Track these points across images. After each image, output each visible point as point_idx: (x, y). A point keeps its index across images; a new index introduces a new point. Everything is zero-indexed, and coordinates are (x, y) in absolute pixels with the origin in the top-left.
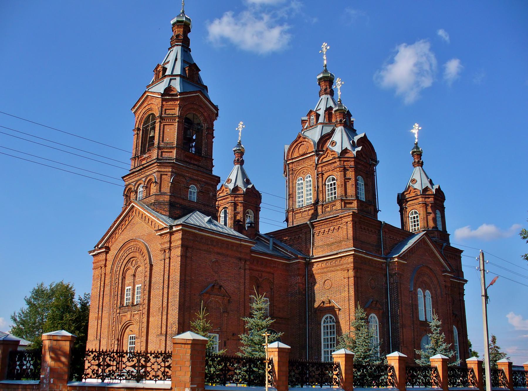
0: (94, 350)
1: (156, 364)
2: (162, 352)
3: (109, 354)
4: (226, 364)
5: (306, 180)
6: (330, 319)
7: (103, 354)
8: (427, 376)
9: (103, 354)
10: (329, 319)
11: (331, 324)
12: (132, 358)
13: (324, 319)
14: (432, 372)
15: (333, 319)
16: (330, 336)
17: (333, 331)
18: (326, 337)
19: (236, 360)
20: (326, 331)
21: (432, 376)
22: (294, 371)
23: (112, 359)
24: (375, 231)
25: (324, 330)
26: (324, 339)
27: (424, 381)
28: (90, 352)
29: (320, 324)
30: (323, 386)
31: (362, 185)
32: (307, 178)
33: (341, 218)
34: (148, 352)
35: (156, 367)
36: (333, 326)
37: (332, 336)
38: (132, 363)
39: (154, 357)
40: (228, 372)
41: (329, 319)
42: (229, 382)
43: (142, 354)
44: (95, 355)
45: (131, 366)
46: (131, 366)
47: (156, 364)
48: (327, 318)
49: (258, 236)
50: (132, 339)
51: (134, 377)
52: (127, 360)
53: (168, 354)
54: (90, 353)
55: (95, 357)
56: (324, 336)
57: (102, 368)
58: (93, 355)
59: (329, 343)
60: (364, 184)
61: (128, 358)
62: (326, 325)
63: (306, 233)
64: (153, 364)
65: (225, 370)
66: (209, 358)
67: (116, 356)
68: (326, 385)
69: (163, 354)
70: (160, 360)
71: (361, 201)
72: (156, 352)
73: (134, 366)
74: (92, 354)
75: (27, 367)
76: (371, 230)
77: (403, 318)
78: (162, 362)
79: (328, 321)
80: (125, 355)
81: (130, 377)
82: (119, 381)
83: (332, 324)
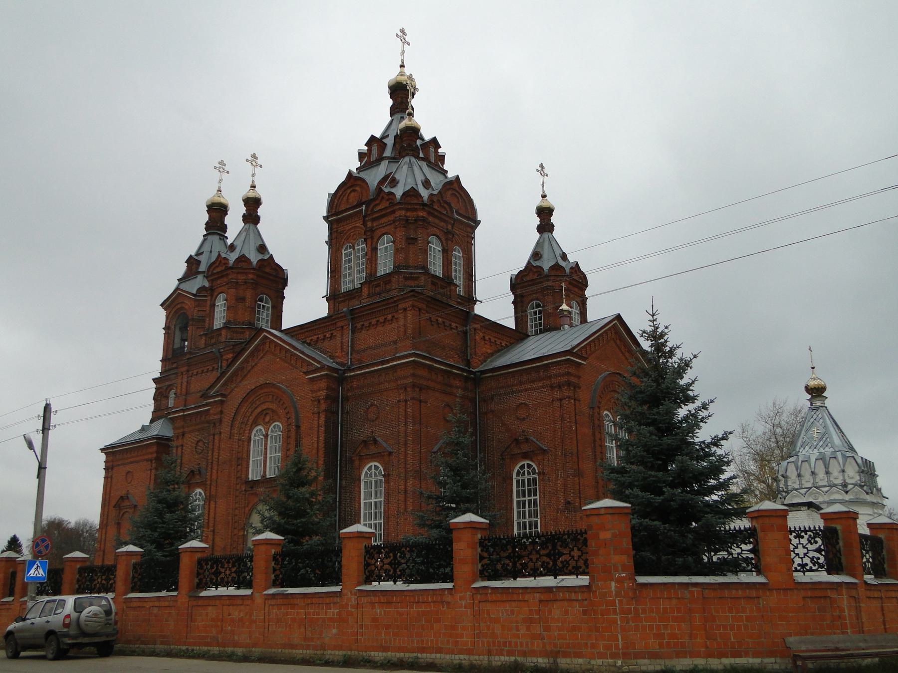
0: (807, 529)
1: (800, 546)
4: (395, 556)
5: (356, 248)
6: (527, 467)
8: (213, 574)
10: (526, 469)
11: (529, 477)
12: (814, 538)
13: (517, 468)
14: (209, 567)
15: (534, 468)
16: (529, 496)
18: (521, 499)
19: (408, 549)
20: (521, 488)
25: (518, 486)
26: (518, 502)
29: (511, 479)
30: (219, 589)
31: (439, 251)
32: (359, 245)
33: (395, 302)
36: (535, 479)
37: (532, 498)
38: (815, 546)
41: (526, 469)
47: (800, 546)
48: (522, 467)
49: (265, 333)
50: (376, 518)
54: (579, 537)
56: (518, 496)
59: (527, 509)
60: (440, 250)
62: (521, 478)
63: (342, 327)
64: (797, 548)
66: (406, 549)
70: (804, 541)
71: (434, 276)
74: (806, 534)
75: (101, 578)
78: (807, 544)
79: (371, 474)
80: (803, 534)
81: (817, 567)
82: (802, 574)
83: (532, 476)
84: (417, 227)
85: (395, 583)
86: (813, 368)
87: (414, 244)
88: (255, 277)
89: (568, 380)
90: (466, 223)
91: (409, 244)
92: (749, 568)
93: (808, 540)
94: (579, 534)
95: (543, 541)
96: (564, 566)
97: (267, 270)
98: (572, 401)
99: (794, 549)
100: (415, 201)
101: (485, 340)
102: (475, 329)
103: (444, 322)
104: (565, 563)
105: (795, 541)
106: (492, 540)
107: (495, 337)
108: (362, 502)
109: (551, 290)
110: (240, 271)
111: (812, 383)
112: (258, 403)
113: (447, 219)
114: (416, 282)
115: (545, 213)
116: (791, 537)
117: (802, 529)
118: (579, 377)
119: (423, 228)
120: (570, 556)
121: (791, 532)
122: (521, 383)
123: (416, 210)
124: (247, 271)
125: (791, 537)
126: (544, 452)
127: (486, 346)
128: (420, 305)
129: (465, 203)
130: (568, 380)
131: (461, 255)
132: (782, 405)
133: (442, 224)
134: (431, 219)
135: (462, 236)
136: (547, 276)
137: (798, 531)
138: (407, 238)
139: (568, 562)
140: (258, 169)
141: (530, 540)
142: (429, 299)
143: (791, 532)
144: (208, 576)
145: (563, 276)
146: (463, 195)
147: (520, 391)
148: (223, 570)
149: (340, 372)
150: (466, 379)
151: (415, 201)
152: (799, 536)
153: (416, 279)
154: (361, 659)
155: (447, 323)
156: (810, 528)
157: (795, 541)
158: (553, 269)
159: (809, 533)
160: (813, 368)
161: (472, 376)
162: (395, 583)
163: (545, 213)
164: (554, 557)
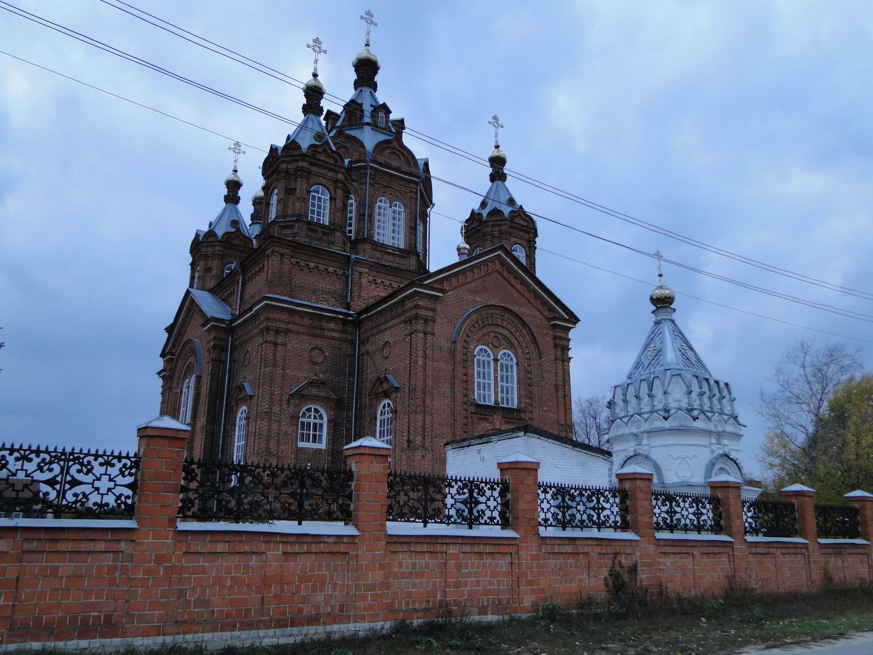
0: (458, 479)
2: (41, 449)
3: (78, 458)
7: (63, 457)
9: (63, 457)
11: (316, 421)
12: (51, 463)
13: (381, 408)
17: (316, 431)
21: (745, 517)
22: (579, 511)
23: (85, 470)
24: (382, 282)
27: (824, 529)
28: (115, 457)
30: (428, 525)
34: (193, 460)
35: (581, 508)
39: (268, 475)
40: (701, 516)
42: (433, 521)
43: (76, 455)
44: (125, 465)
45: (81, 483)
46: (81, 483)
51: (464, 519)
52: (37, 468)
53: (464, 482)
55: (124, 469)
57: (58, 489)
58: (121, 465)
61: (120, 470)
64: (99, 479)
65: (564, 507)
67: (94, 463)
68: (436, 522)
69: (42, 452)
72: (109, 453)
73: (75, 483)
74: (120, 461)
76: (382, 282)
77: (421, 424)
84: (297, 178)
85: (425, 526)
86: (661, 275)
87: (293, 194)
88: (221, 249)
89: (417, 313)
90: (408, 179)
91: (289, 194)
92: (459, 521)
93: (457, 490)
94: (453, 481)
95: (589, 494)
96: (571, 519)
97: (236, 242)
98: (421, 335)
99: (497, 506)
100: (296, 153)
101: (376, 283)
102: (361, 273)
103: (317, 267)
104: (481, 513)
105: (542, 496)
106: (578, 489)
107: (390, 280)
108: (236, 444)
109: (489, 235)
110: (209, 244)
111: (659, 293)
112: (187, 357)
113: (337, 168)
114: (292, 230)
115: (498, 163)
116: (539, 491)
117: (454, 478)
118: (434, 310)
119: (302, 177)
120: (486, 506)
121: (540, 486)
122: (386, 322)
123: (297, 161)
124: (215, 244)
125: (539, 491)
126: (397, 389)
127: (378, 289)
128: (283, 251)
129: (408, 159)
130: (417, 313)
131: (403, 210)
132: (809, 345)
133: (330, 174)
134: (315, 169)
135: (404, 192)
136: (486, 221)
137: (492, 483)
138: (286, 189)
139: (483, 512)
140: (241, 156)
141: (578, 492)
142: (294, 244)
143: (540, 486)
144: (659, 514)
145: (502, 220)
146: (405, 153)
147: (386, 330)
148: (678, 509)
149: (226, 322)
150: (345, 322)
151: (296, 153)
152: (545, 492)
153: (292, 227)
154: (726, 581)
155: (322, 267)
156: (461, 478)
157: (542, 496)
158: (492, 215)
159: (459, 483)
160: (661, 275)
161: (350, 318)
162: (425, 526)
163: (498, 163)
164: (471, 506)
